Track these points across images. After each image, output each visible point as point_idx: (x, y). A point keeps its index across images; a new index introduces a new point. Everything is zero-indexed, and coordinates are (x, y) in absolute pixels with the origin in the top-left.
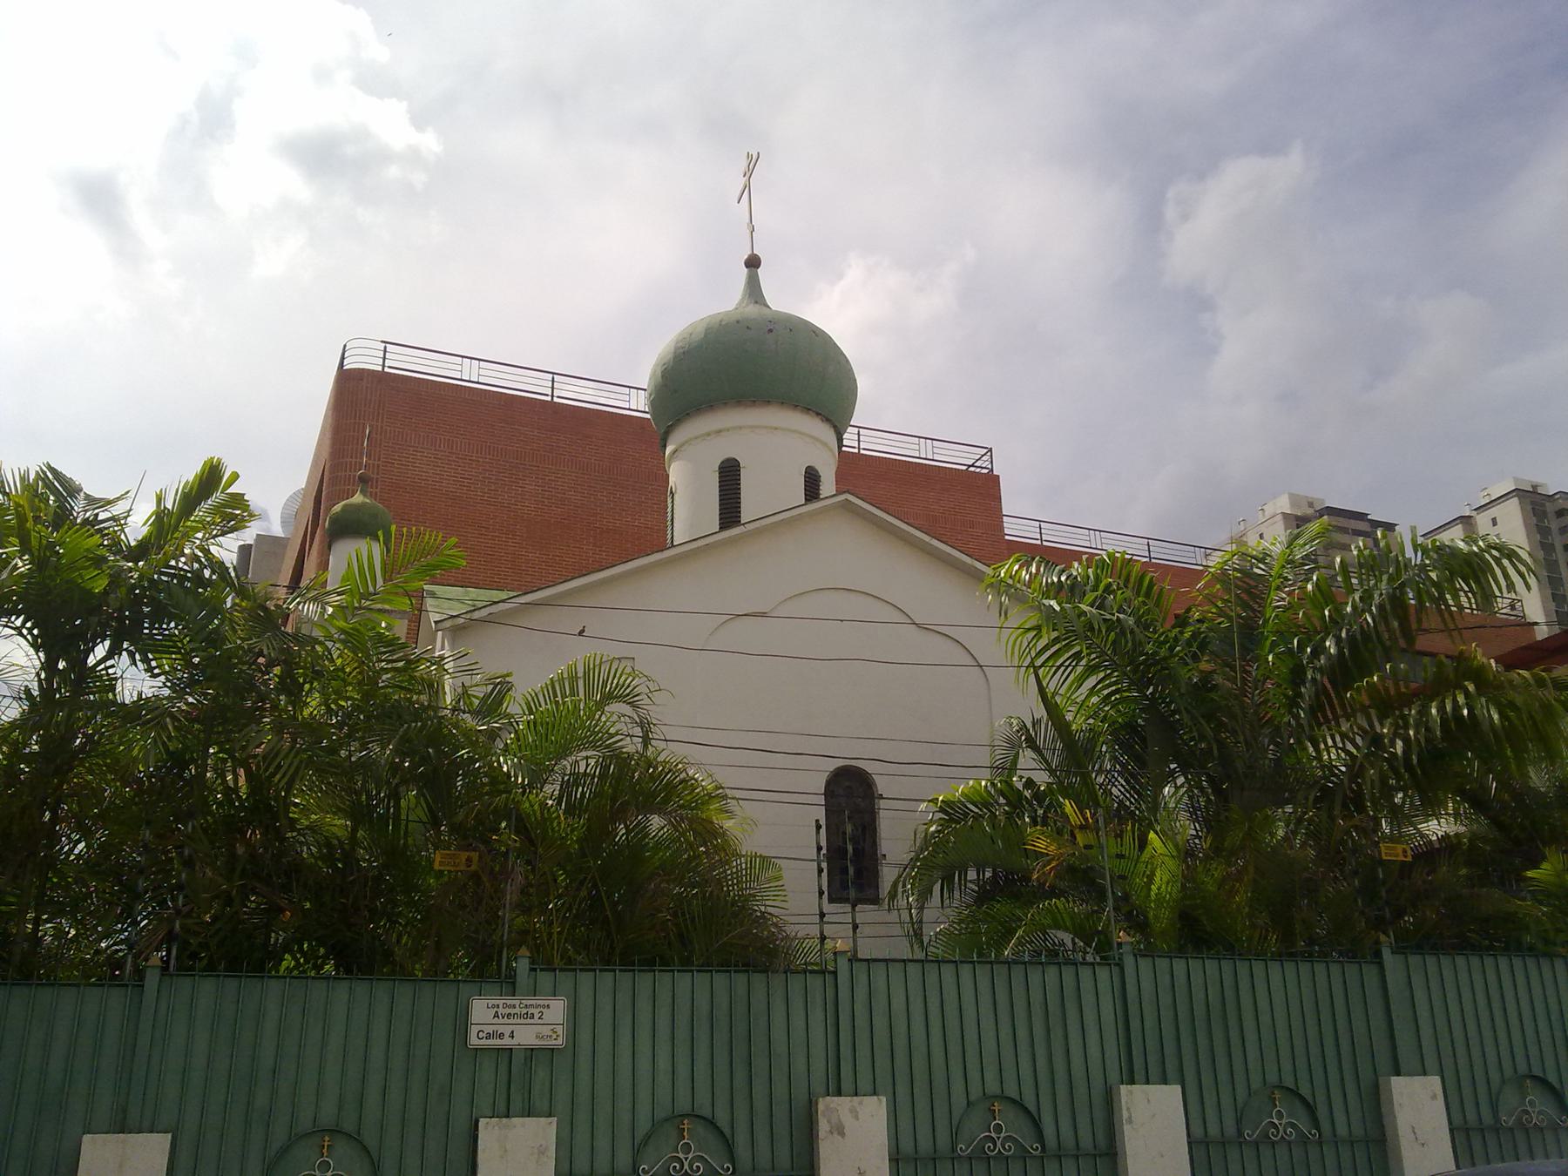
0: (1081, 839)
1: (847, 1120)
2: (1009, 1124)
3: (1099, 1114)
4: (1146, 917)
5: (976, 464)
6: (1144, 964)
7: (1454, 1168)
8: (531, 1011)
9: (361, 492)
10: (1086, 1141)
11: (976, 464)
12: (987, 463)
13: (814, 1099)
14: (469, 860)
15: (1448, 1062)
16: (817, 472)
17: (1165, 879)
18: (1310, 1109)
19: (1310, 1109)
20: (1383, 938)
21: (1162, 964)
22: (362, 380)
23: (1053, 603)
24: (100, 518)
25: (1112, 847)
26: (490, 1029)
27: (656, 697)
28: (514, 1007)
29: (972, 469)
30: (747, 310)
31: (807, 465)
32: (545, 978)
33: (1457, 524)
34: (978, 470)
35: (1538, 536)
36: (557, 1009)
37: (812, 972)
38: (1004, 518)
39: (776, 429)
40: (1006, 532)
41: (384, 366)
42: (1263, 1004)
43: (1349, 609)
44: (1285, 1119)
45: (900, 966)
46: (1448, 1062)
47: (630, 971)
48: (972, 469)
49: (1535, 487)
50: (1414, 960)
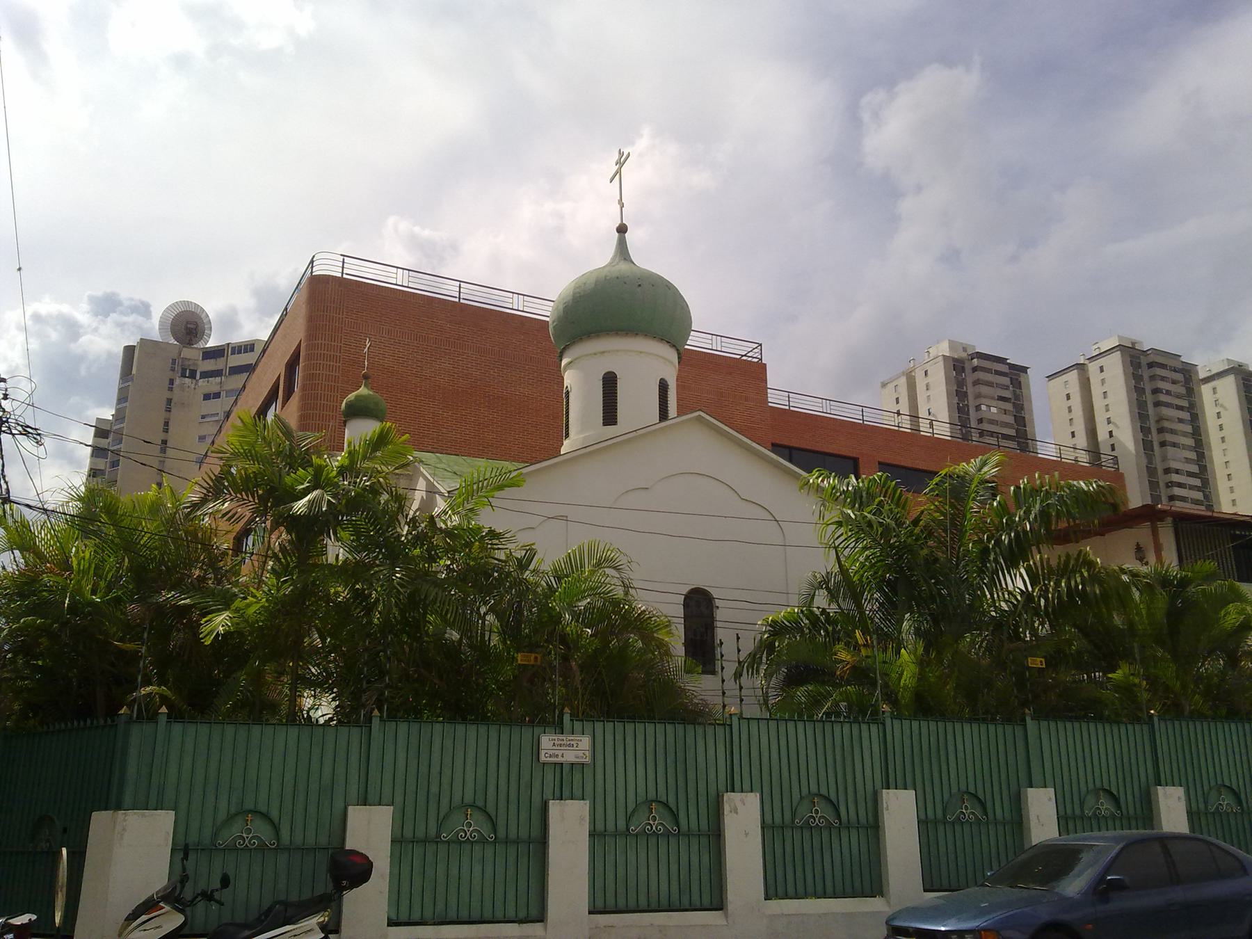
0: (864, 652)
1: (739, 805)
2: (822, 811)
3: (870, 804)
4: (897, 697)
5: (748, 355)
6: (897, 723)
7: (1058, 836)
8: (572, 743)
9: (365, 385)
10: (863, 820)
11: (748, 355)
12: (757, 354)
13: (721, 794)
14: (536, 658)
15: (1058, 781)
16: (666, 382)
17: (908, 676)
18: (983, 804)
19: (983, 804)
20: (1027, 711)
21: (906, 723)
22: (328, 283)
23: (849, 512)
25: (880, 656)
26: (551, 752)
27: (634, 566)
28: (563, 740)
29: (744, 358)
30: (618, 268)
31: (661, 377)
32: (578, 725)
33: (1074, 369)
34: (750, 359)
35: (1133, 381)
36: (585, 742)
37: (718, 724)
38: (769, 390)
39: (641, 352)
40: (769, 401)
41: (342, 273)
42: (960, 747)
43: (1017, 519)
44: (969, 810)
45: (756, 721)
46: (1058, 781)
47: (643, 722)
48: (744, 358)
49: (1133, 344)
50: (1044, 724)
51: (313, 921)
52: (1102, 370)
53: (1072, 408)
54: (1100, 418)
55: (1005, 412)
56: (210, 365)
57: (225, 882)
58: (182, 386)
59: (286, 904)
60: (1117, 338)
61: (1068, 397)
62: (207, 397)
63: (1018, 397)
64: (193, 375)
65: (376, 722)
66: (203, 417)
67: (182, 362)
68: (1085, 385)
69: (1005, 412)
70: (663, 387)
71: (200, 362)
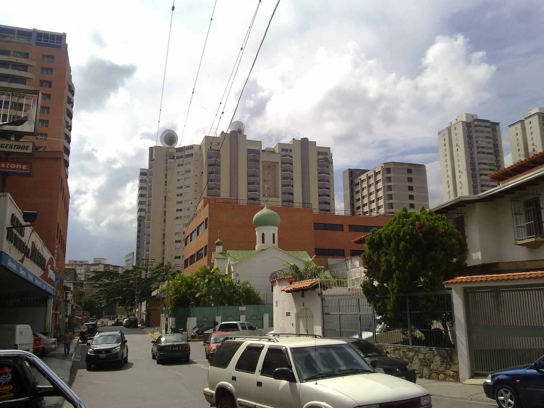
24: (272, 335)
32: (244, 306)
36: (245, 308)
51: (212, 329)
52: (530, 123)
53: (519, 139)
54: (530, 143)
55: (489, 143)
56: (179, 154)
57: (203, 325)
58: (170, 162)
59: (209, 328)
60: (538, 108)
61: (517, 134)
62: (179, 165)
63: (495, 136)
64: (173, 158)
65: (219, 306)
66: (178, 173)
67: (170, 153)
68: (524, 129)
69: (489, 143)
70: (274, 235)
71: (175, 153)
